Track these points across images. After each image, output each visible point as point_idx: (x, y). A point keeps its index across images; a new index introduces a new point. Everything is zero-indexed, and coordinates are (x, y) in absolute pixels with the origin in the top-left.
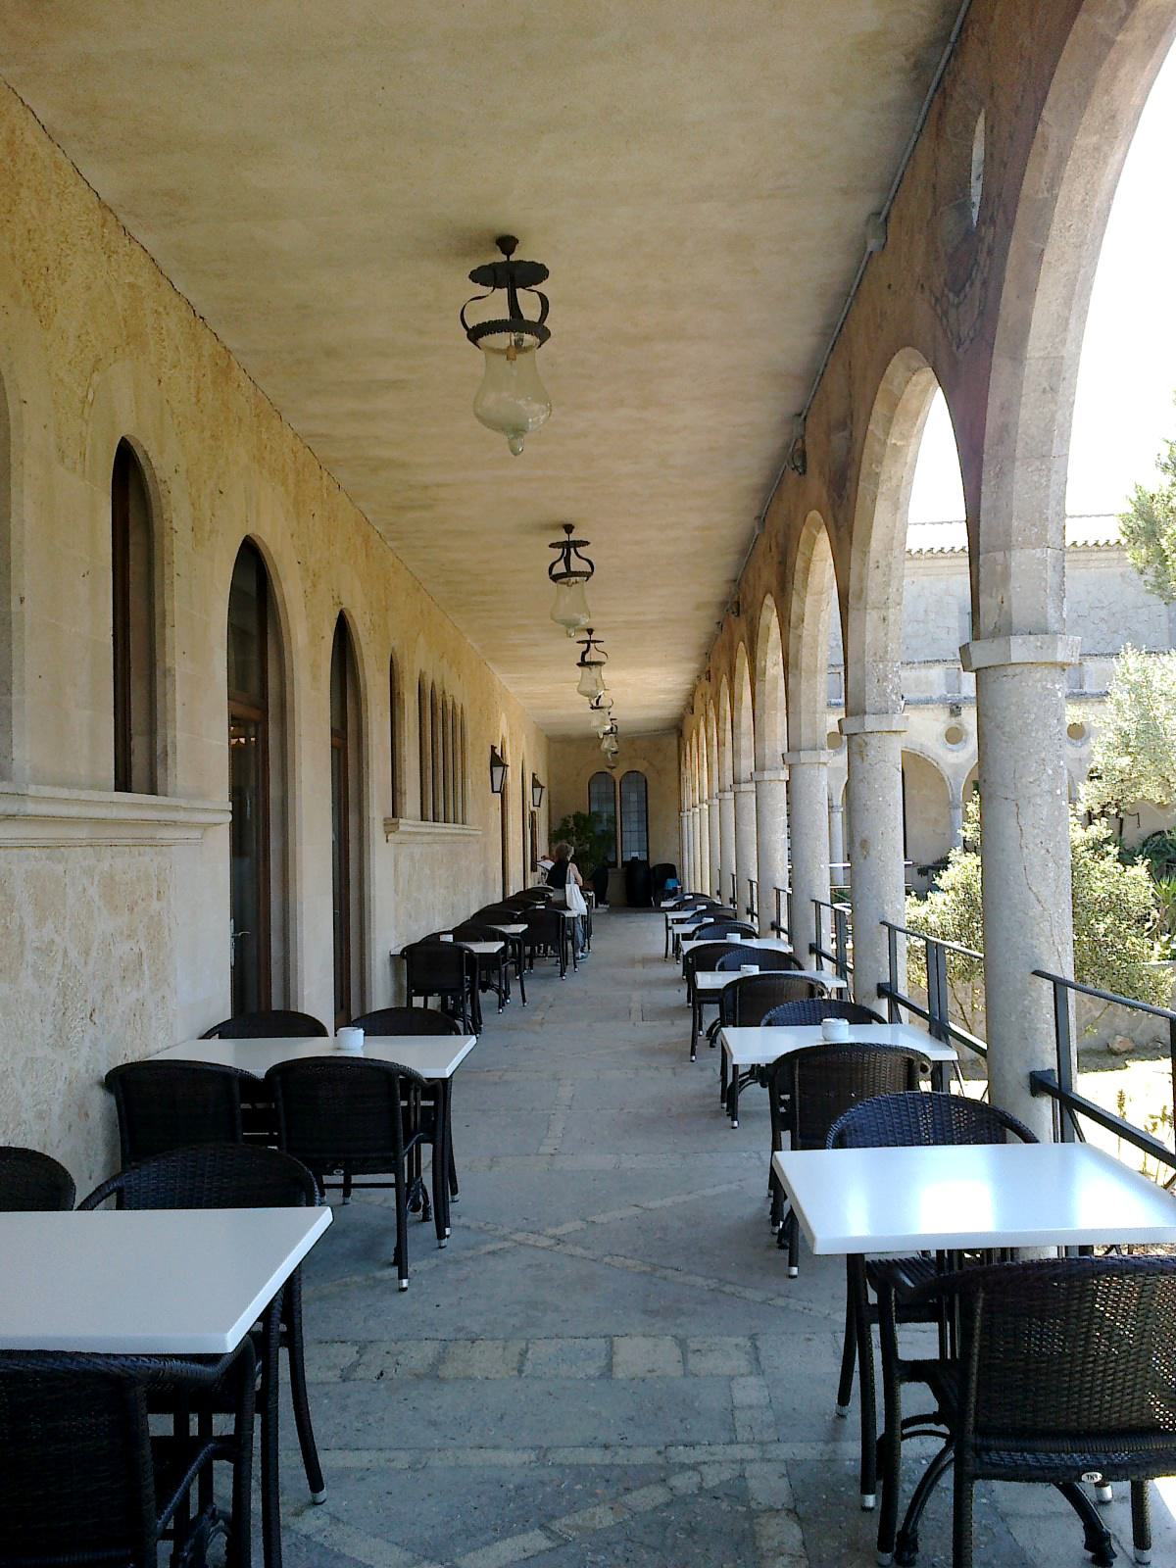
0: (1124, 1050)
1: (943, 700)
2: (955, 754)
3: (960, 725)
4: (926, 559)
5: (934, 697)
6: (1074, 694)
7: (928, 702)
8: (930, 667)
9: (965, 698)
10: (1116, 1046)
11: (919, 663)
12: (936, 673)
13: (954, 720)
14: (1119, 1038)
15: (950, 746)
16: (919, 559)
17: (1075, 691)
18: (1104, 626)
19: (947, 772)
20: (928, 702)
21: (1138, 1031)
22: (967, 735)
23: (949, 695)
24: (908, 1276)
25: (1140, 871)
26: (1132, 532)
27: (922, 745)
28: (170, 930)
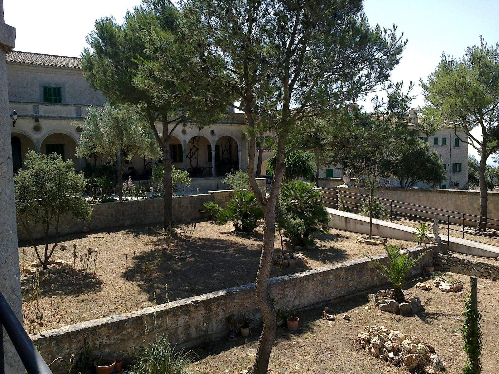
0: (86, 231)
1: (32, 116)
2: (37, 135)
3: (39, 125)
4: (26, 66)
5: (29, 115)
6: (78, 117)
7: (27, 116)
8: (27, 104)
9: (40, 116)
10: (84, 230)
11: (23, 102)
12: (30, 107)
13: (36, 124)
14: (85, 228)
15: (35, 132)
16: (23, 65)
17: (79, 116)
18: (89, 96)
19: (35, 141)
20: (27, 116)
21: (91, 225)
22: (41, 128)
23: (35, 115)
24: (395, 216)
25: (81, 176)
26: (85, 67)
27: (25, 131)
28: (191, 150)
